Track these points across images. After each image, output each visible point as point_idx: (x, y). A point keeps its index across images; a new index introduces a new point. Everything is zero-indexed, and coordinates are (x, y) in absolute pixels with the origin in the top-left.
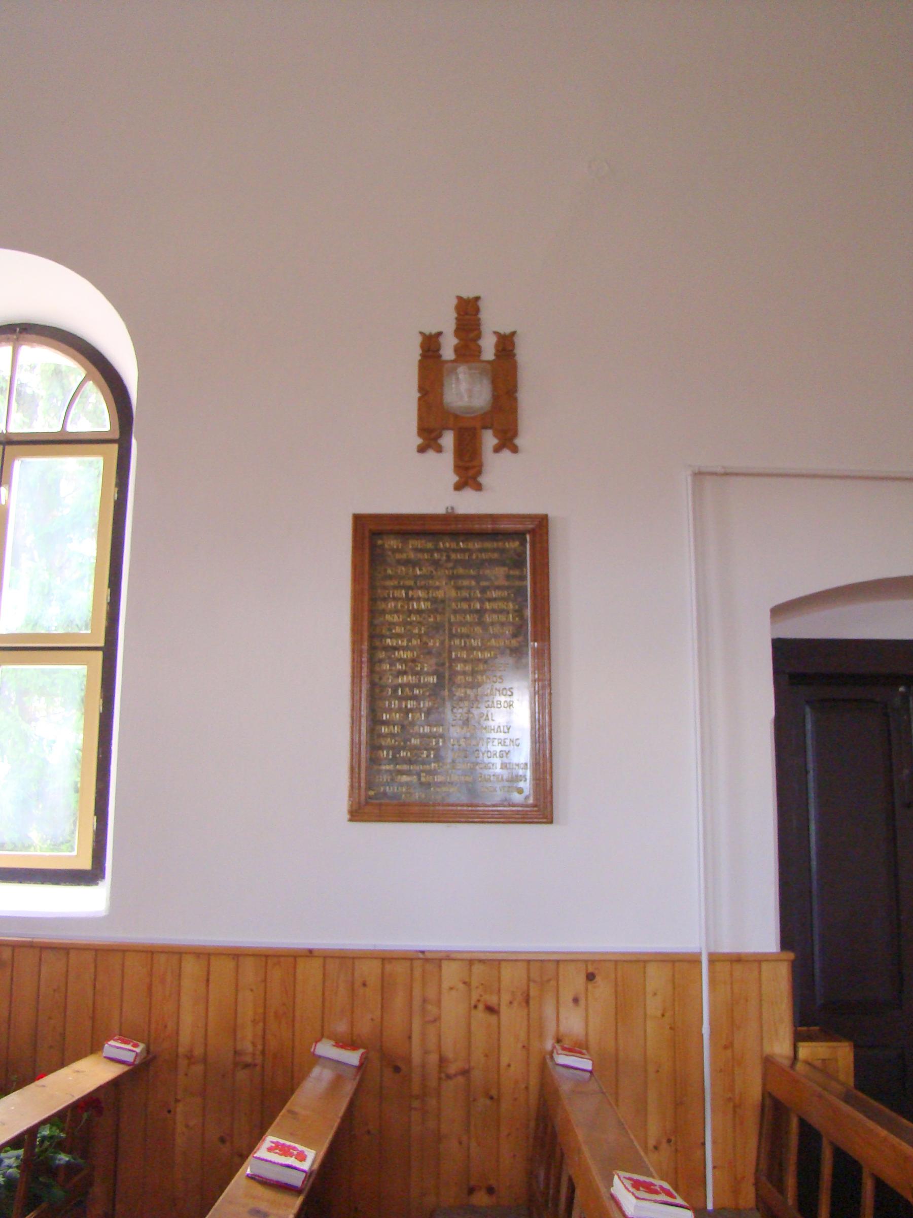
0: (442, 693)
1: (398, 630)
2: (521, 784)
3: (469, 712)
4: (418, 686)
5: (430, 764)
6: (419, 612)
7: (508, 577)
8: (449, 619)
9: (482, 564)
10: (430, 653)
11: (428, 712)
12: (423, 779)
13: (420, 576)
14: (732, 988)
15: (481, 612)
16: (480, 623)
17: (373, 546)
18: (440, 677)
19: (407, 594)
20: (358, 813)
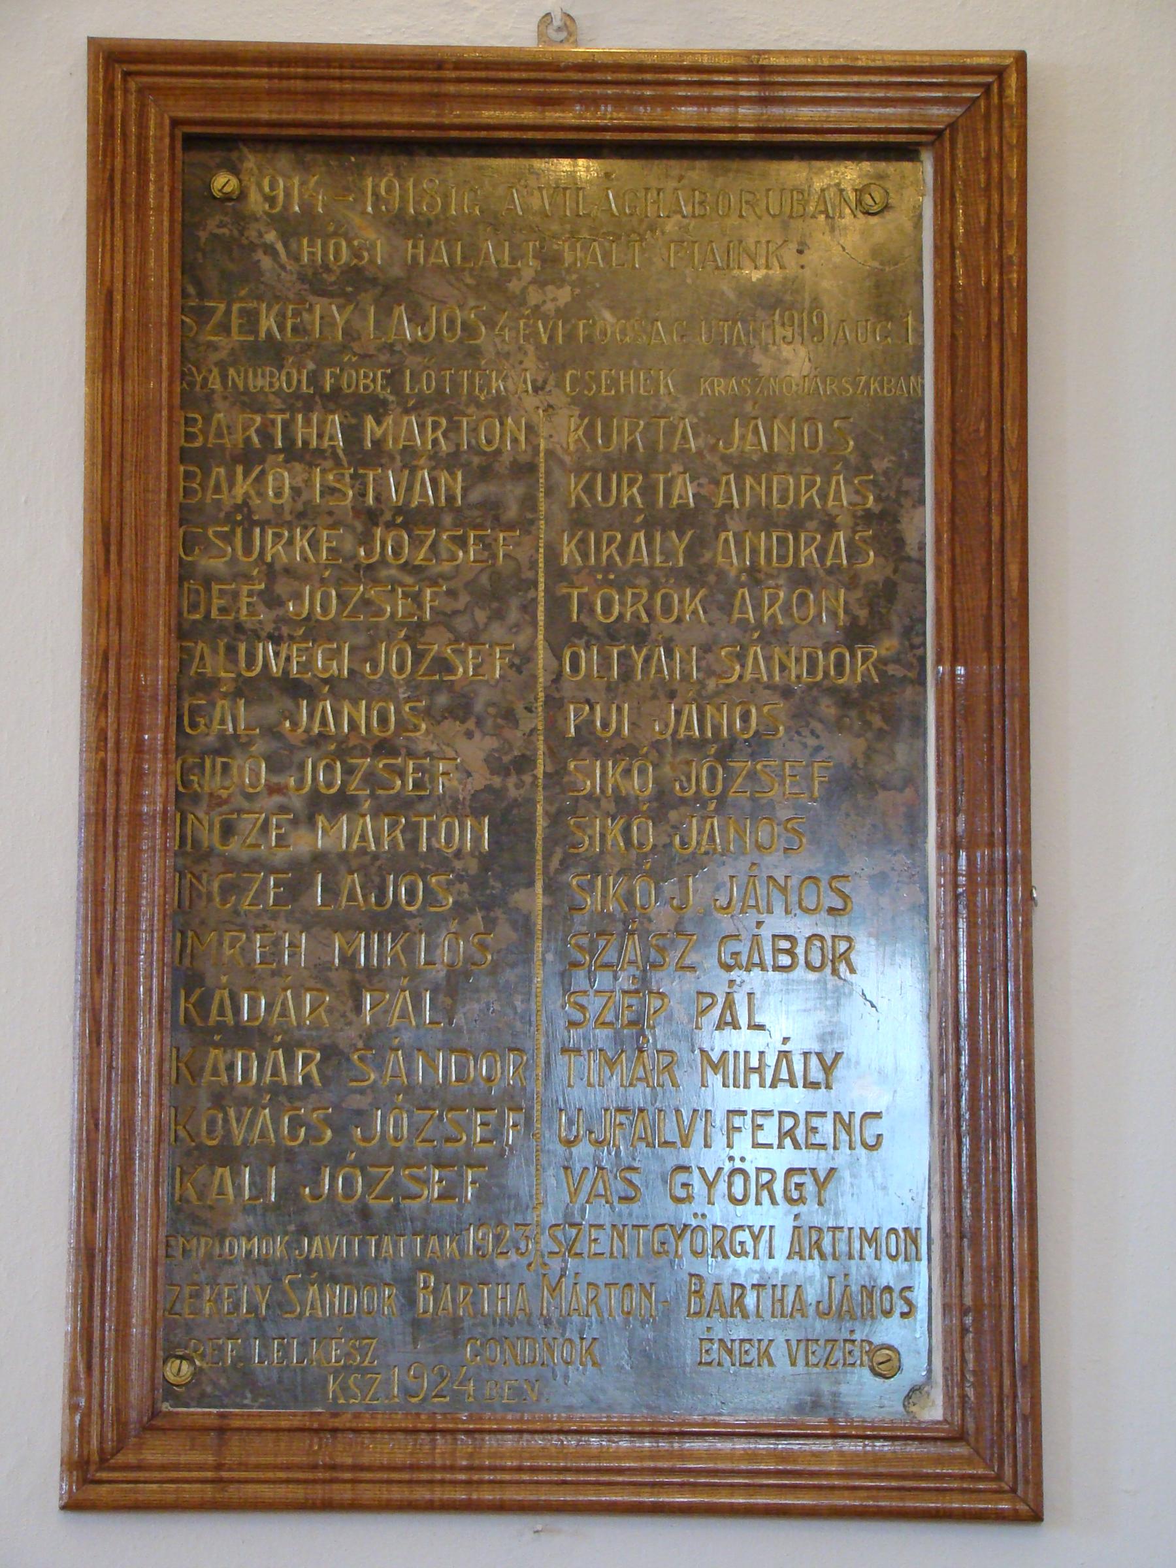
0: (519, 898)
1: (309, 602)
2: (890, 1331)
3: (643, 987)
4: (407, 862)
5: (458, 1233)
6: (411, 519)
8: (553, 554)
10: (461, 708)
11: (455, 986)
12: (425, 1302)
13: (416, 347)
16: (695, 574)
17: (194, 202)
18: (510, 824)
19: (353, 433)
20: (106, 1472)
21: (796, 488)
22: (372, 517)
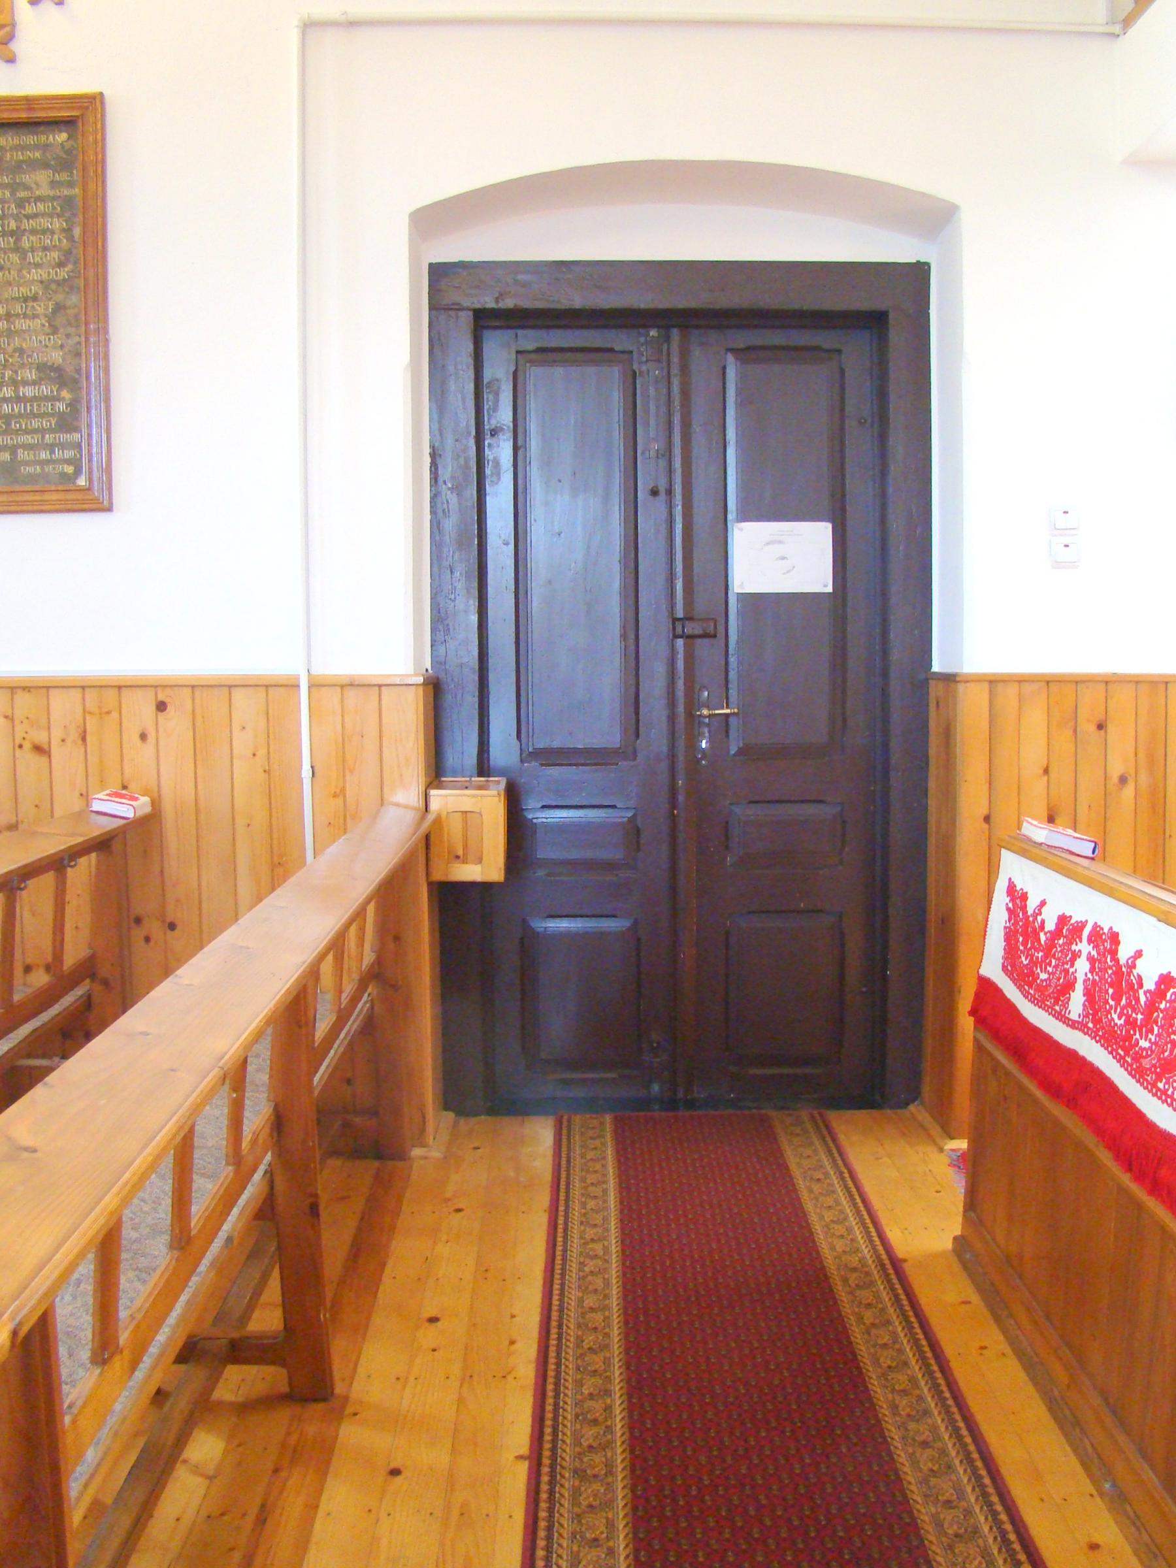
7: (53, 184)
9: (18, 167)
14: (343, 721)
15: (17, 234)
16: (17, 249)
21: (45, 223)
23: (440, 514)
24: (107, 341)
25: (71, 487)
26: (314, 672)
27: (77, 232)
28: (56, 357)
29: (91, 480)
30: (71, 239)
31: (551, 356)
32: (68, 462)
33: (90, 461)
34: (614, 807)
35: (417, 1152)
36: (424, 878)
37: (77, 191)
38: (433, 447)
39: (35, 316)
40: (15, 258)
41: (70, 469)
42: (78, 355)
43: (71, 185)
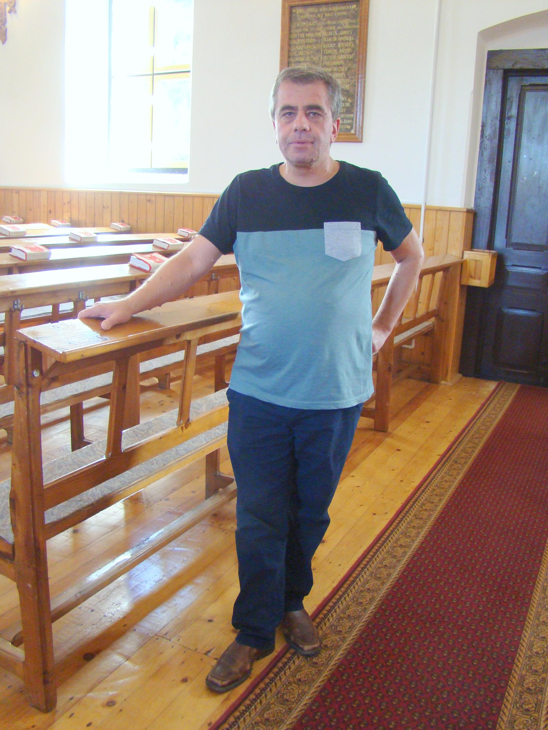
1: (301, 53)
6: (310, 44)
7: (350, 24)
9: (339, 18)
19: (305, 36)
21: (346, 38)
22: (306, 44)
23: (483, 148)
24: (365, 82)
25: (348, 133)
26: (427, 204)
27: (357, 41)
28: (347, 87)
29: (356, 131)
30: (355, 44)
31: (535, 88)
32: (348, 124)
33: (356, 124)
34: (540, 268)
35: (443, 382)
36: (458, 282)
37: (358, 26)
38: (483, 123)
39: (341, 72)
40: (335, 51)
41: (349, 127)
42: (355, 86)
43: (356, 24)
